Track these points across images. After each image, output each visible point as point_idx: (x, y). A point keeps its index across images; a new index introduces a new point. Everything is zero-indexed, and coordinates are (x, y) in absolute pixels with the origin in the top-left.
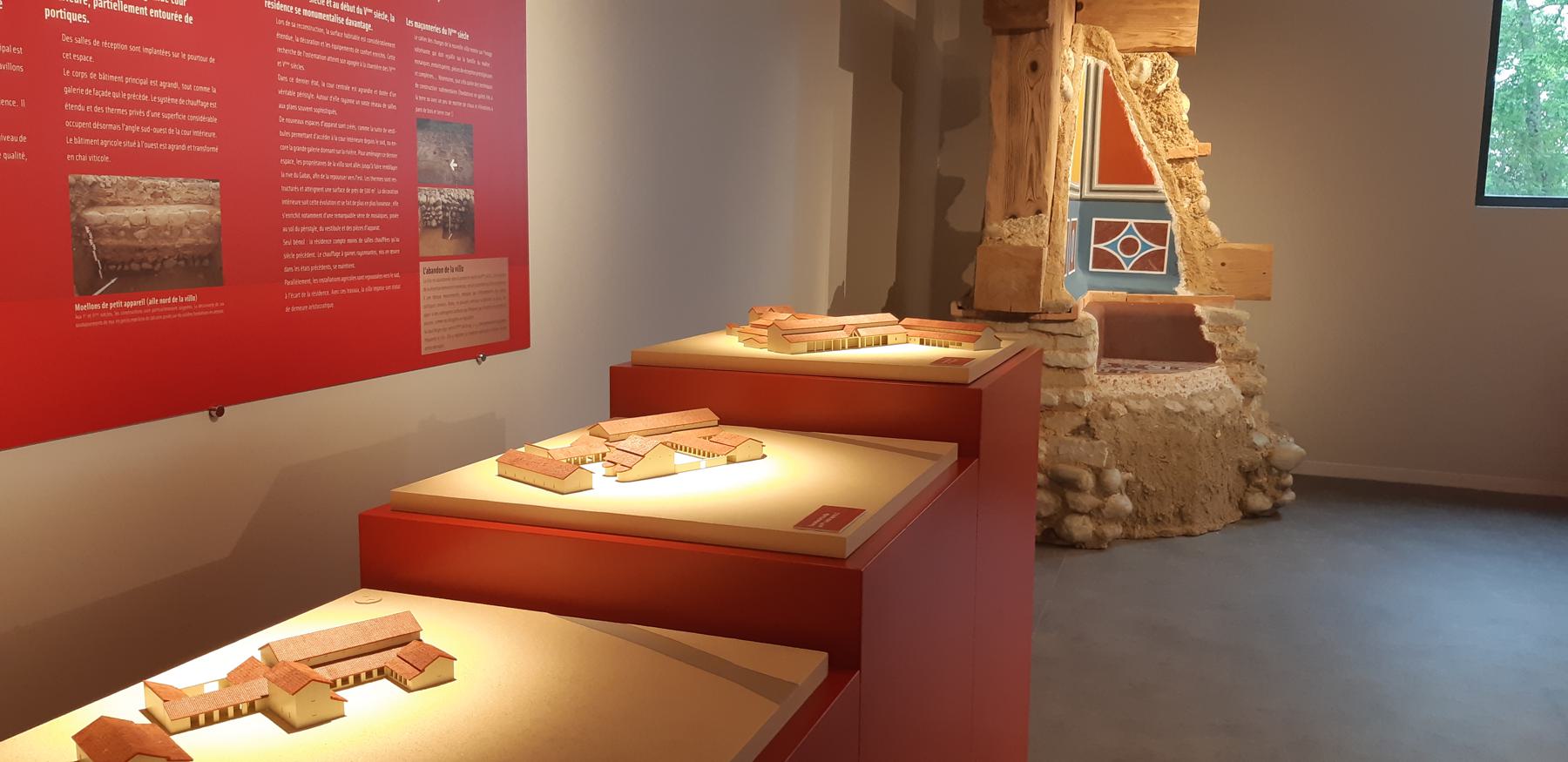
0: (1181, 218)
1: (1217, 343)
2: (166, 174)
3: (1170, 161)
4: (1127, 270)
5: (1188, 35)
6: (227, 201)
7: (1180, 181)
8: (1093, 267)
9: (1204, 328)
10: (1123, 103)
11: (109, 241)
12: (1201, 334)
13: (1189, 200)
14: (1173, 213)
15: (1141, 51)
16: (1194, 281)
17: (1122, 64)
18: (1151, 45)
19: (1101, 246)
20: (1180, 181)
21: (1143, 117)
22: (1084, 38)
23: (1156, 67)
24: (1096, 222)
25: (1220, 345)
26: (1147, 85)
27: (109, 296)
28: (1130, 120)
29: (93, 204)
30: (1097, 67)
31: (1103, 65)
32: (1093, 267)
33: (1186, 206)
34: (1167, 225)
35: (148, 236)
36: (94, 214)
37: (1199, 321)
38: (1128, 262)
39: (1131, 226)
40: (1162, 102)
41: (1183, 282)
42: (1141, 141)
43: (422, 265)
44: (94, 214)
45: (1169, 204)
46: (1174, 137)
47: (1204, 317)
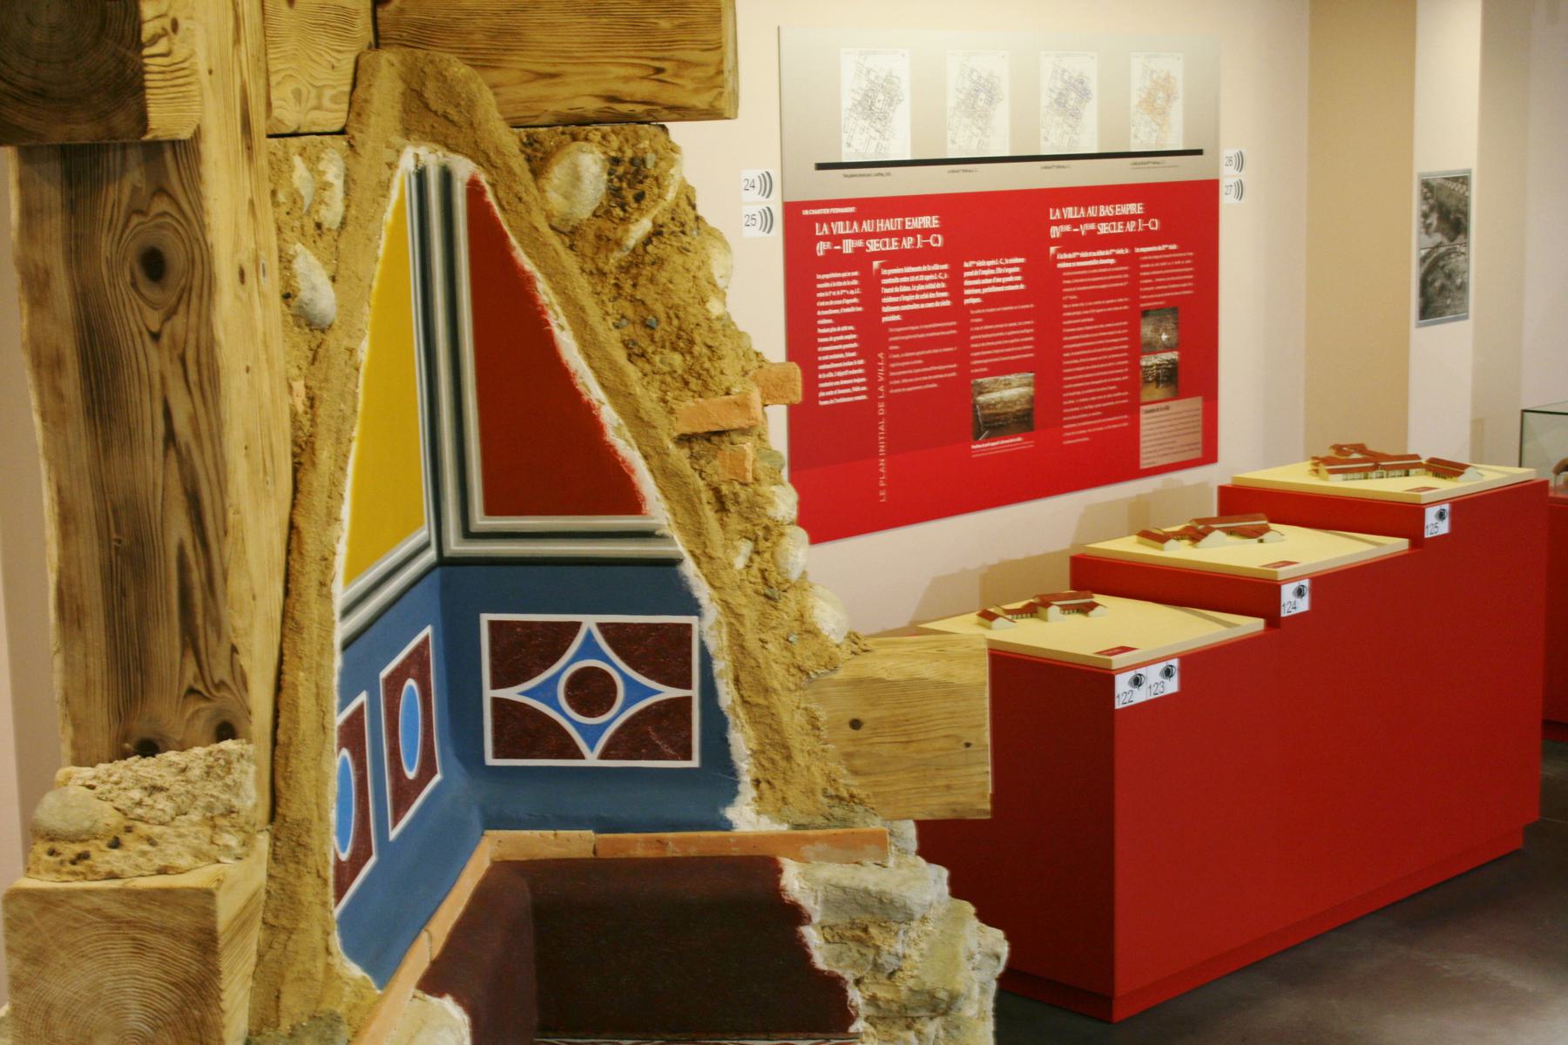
0: (726, 605)
1: (849, 976)
2: (1009, 372)
3: (685, 440)
4: (592, 759)
5: (699, 73)
6: (1037, 384)
7: (716, 491)
8: (497, 755)
9: (811, 935)
10: (529, 280)
11: (987, 412)
12: (801, 952)
13: (746, 547)
14: (702, 592)
15: (576, 124)
16: (778, 783)
17: (519, 164)
18: (600, 104)
19: (512, 693)
20: (716, 491)
21: (594, 314)
22: (400, 87)
23: (620, 170)
24: (492, 624)
25: (858, 982)
26: (599, 222)
27: (988, 439)
28: (557, 331)
29: (981, 393)
30: (447, 177)
31: (464, 169)
32: (497, 755)
33: (740, 562)
34: (688, 627)
35: (1002, 407)
36: (981, 399)
37: (796, 914)
38: (591, 735)
39: (589, 635)
40: (647, 271)
41: (747, 791)
42: (592, 389)
43: (1143, 408)
44: (981, 399)
45: (689, 568)
46: (690, 369)
47: (809, 903)
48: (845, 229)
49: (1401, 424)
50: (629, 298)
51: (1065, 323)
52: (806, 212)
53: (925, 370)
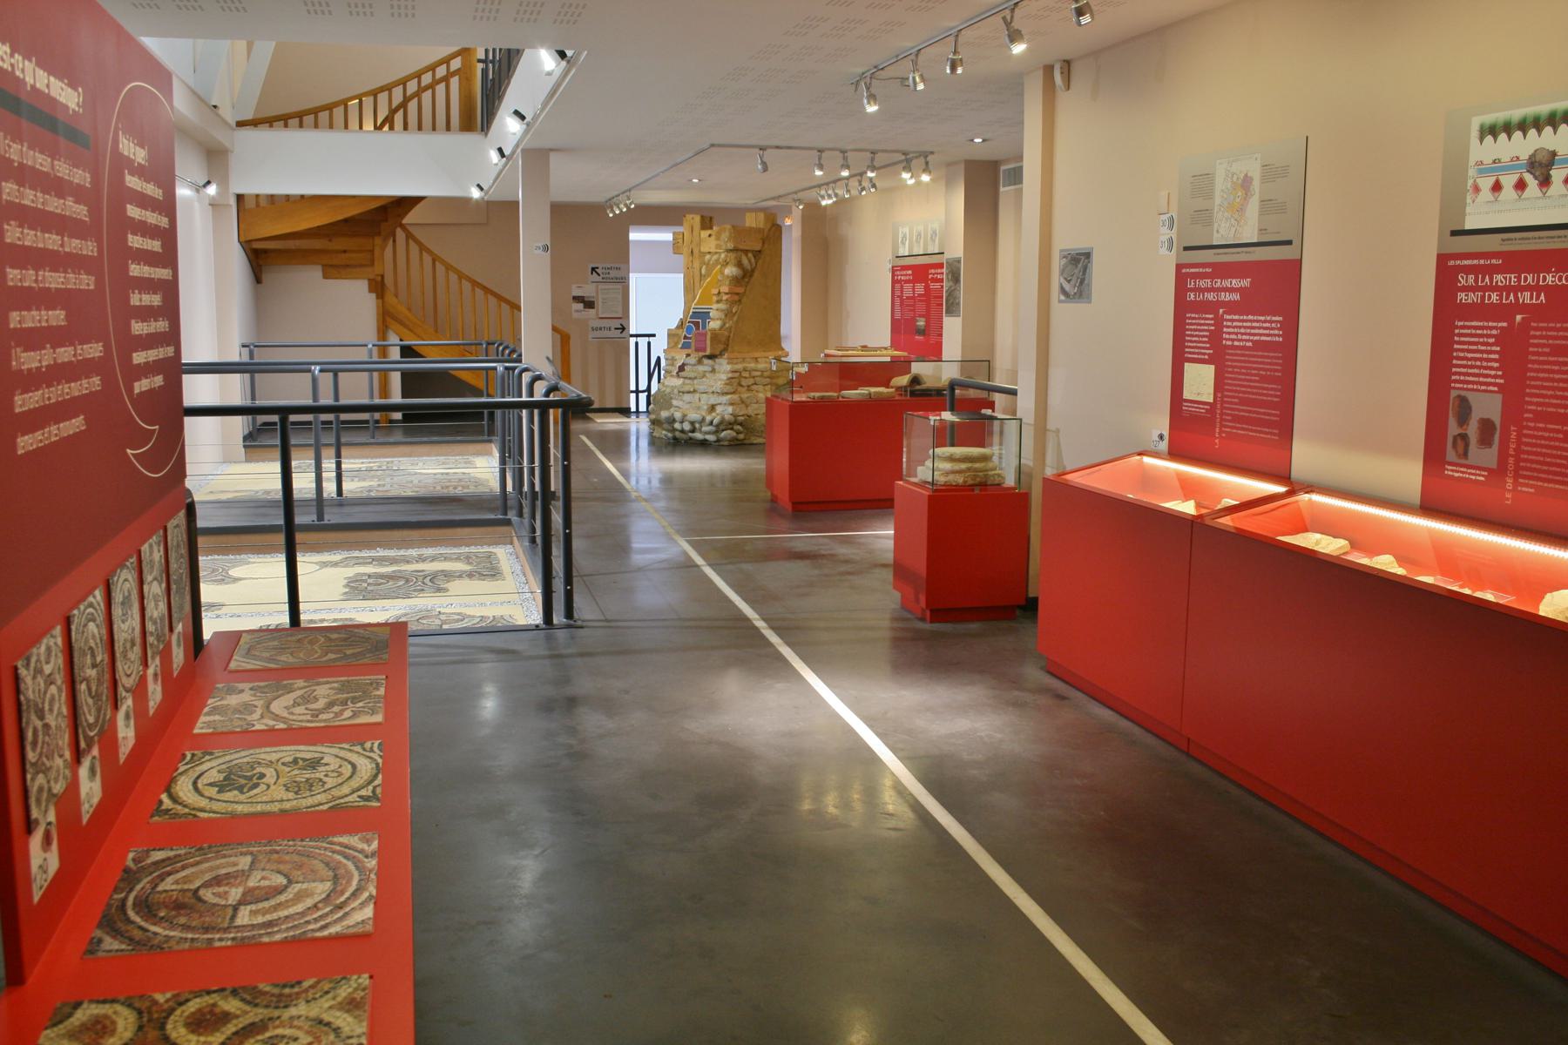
48: (1531, 298)
49: (1065, 468)
50: (191, 878)
51: (1531, 341)
52: (1452, 263)
53: (1551, 359)
